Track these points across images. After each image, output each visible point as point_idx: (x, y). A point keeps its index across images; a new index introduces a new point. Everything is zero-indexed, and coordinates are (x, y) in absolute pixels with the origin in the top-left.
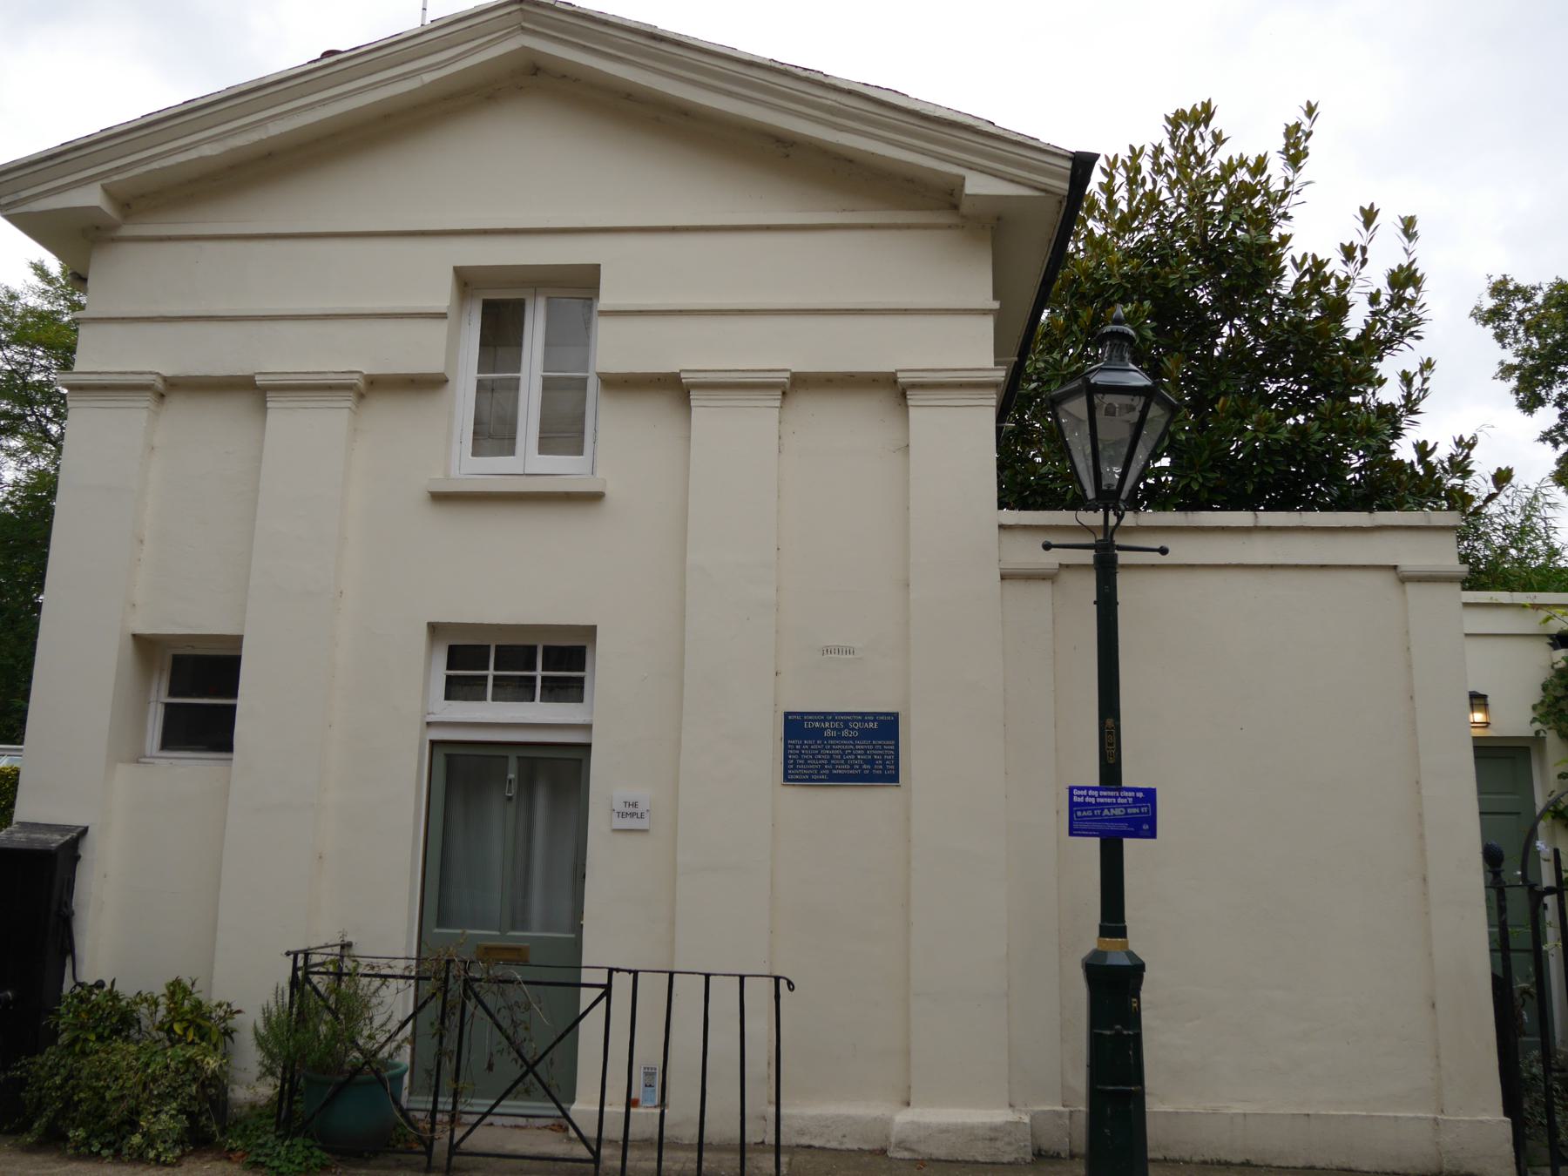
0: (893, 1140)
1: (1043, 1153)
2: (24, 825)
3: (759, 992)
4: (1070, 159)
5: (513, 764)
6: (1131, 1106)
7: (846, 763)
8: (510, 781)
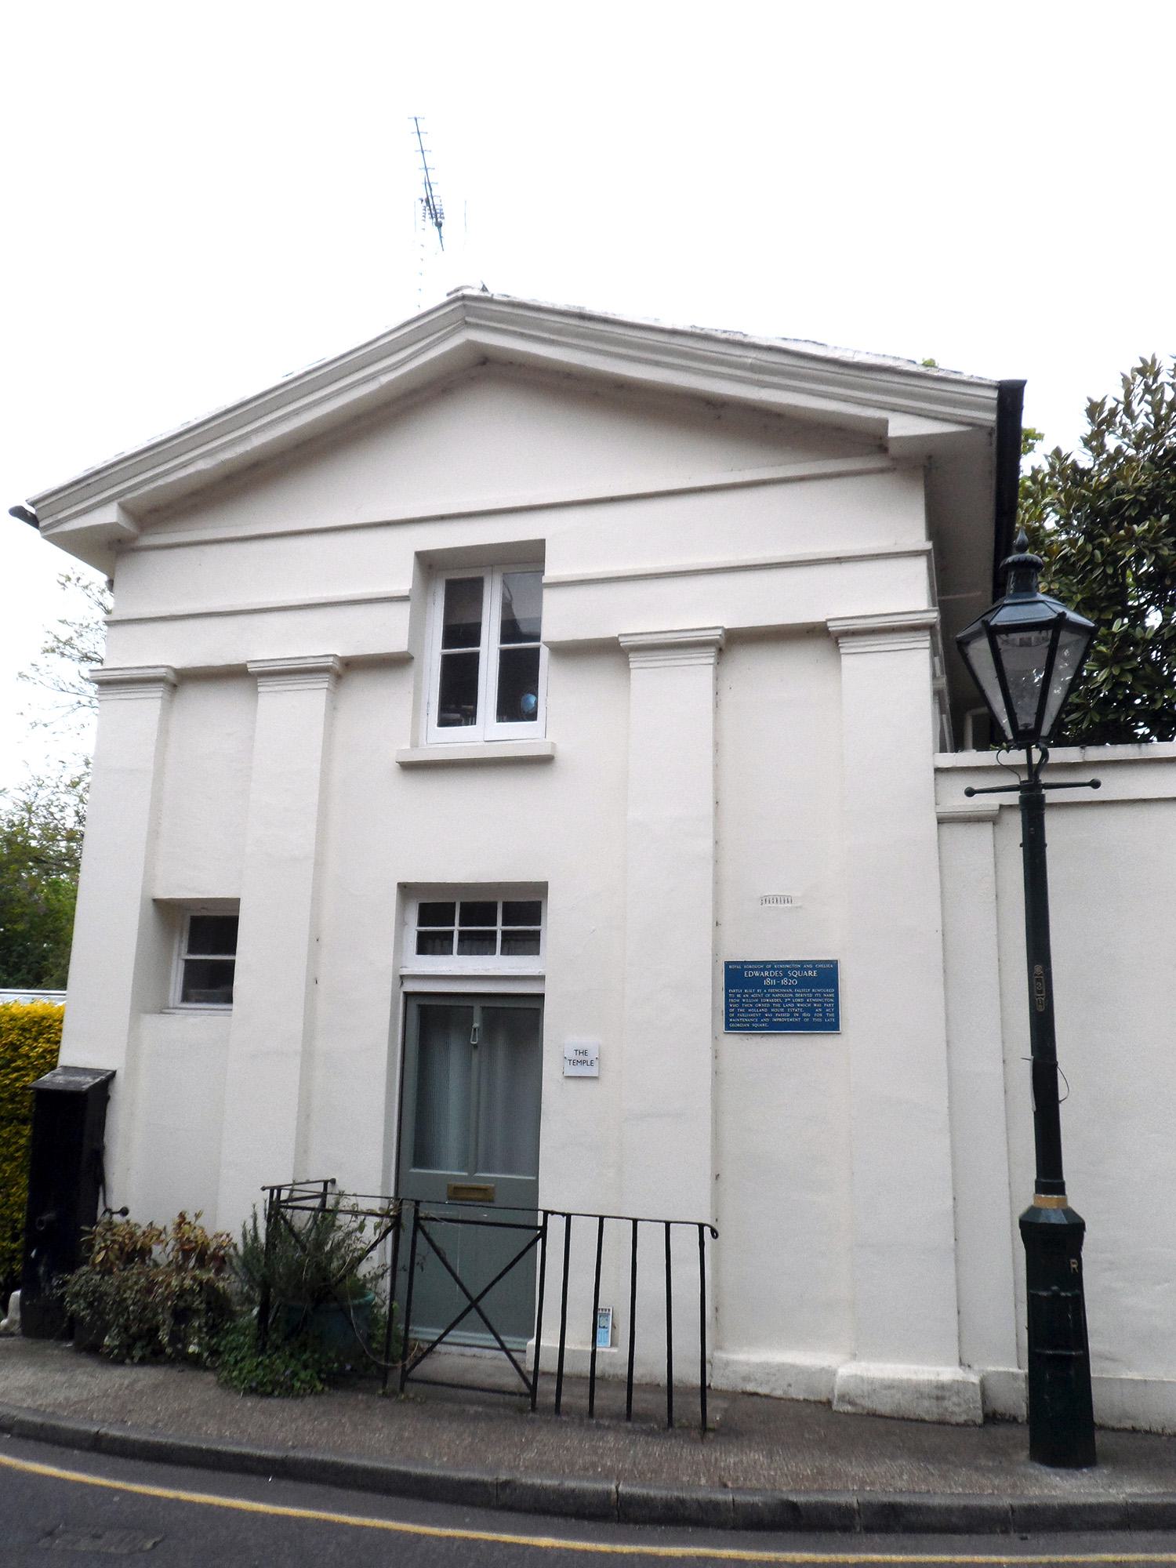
0: (836, 1392)
1: (999, 1417)
2: (66, 1068)
3: (685, 1241)
4: (996, 388)
5: (477, 1014)
6: (1072, 1373)
7: (786, 1012)
8: (475, 1029)
